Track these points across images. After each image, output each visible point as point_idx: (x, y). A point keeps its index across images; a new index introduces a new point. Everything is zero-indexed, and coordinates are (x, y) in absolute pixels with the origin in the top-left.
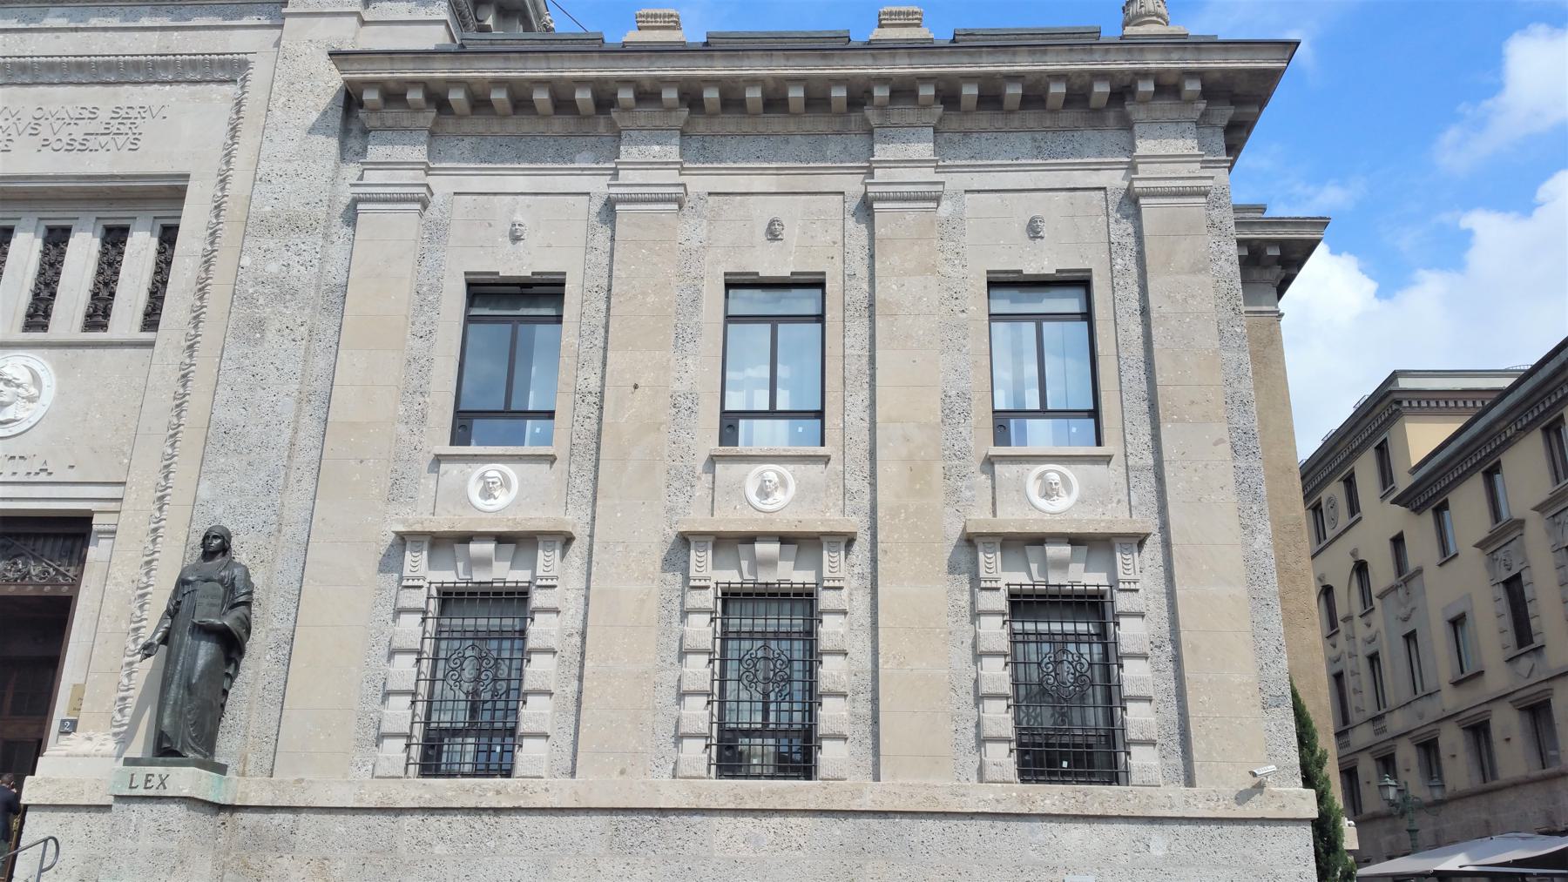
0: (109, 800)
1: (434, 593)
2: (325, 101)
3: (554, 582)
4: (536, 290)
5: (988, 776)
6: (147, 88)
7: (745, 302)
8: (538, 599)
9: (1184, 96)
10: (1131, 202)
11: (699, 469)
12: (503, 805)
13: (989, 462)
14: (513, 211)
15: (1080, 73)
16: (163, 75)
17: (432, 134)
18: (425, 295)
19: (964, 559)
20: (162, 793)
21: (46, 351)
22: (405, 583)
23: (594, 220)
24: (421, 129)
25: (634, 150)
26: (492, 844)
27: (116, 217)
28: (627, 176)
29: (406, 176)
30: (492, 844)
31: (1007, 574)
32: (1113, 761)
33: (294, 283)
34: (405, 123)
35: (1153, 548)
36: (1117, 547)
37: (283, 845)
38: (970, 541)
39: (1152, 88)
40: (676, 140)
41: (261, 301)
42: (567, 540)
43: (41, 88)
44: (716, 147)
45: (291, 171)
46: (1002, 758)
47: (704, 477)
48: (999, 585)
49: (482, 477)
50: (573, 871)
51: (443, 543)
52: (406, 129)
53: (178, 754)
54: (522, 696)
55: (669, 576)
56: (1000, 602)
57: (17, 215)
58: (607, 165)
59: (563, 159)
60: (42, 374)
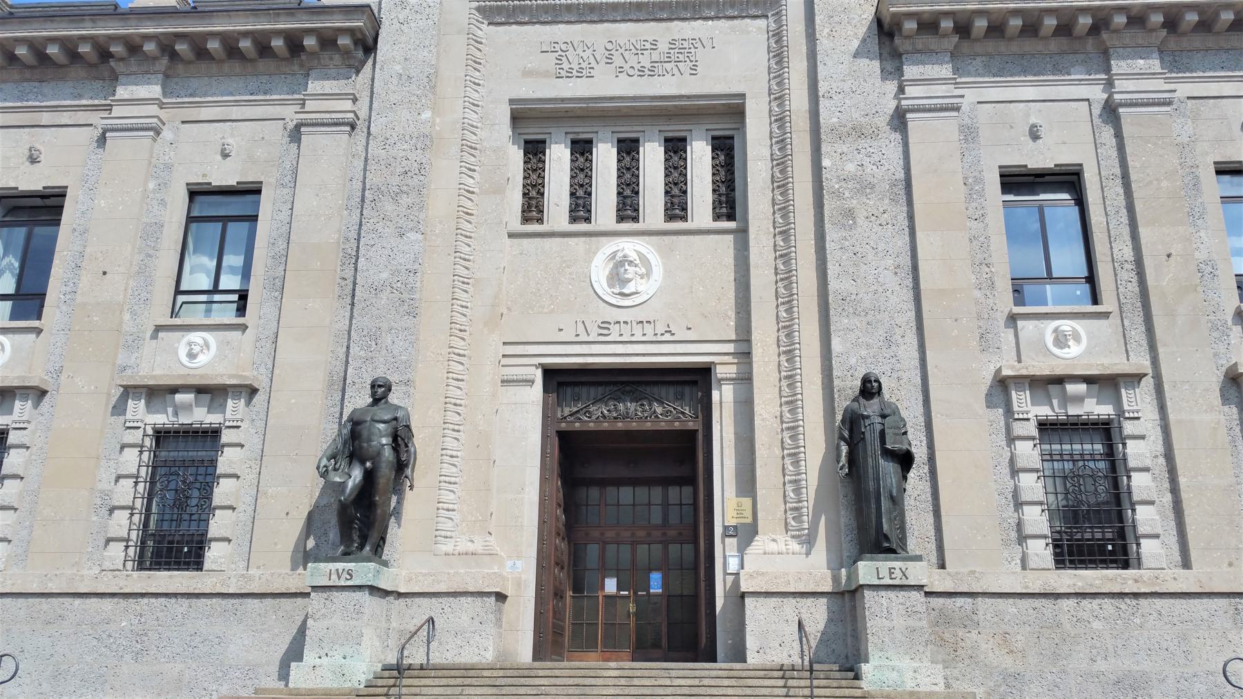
0: (309, 590)
1: (150, 432)
2: (862, 31)
3: (239, 424)
4: (1047, 178)
5: (1032, 564)
6: (693, 23)
7: (206, 207)
8: (226, 437)
9: (1149, 26)
10: (1111, 112)
11: (1230, 323)
12: (1143, 590)
13: (1012, 319)
14: (1028, 115)
15: (1034, 9)
16: (521, 18)
17: (167, 76)
18: (972, 186)
19: (999, 398)
20: (905, 582)
21: (647, 238)
22: (128, 424)
23: (1097, 121)
24: (945, 51)
25: (1123, 63)
26: (1138, 621)
27: (675, 130)
28: (310, 105)
29: (940, 90)
30: (1138, 621)
31: (1031, 409)
32: (1125, 550)
33: (870, 179)
34: (932, 47)
35: (1148, 382)
36: (1122, 384)
37: (969, 622)
38: (1003, 385)
39: (1125, 20)
40: (1156, 55)
41: (847, 195)
42: (253, 391)
43: (606, 24)
44: (1185, 61)
45: (847, 89)
46: (1041, 551)
47: (1234, 328)
48: (1030, 416)
49: (1056, 330)
50: (1209, 642)
51: (156, 394)
52: (932, 51)
53: (894, 552)
54: (211, 510)
55: (1226, 408)
56: (1031, 429)
57: (595, 129)
58: (1098, 76)
59: (1060, 72)
60: (649, 256)
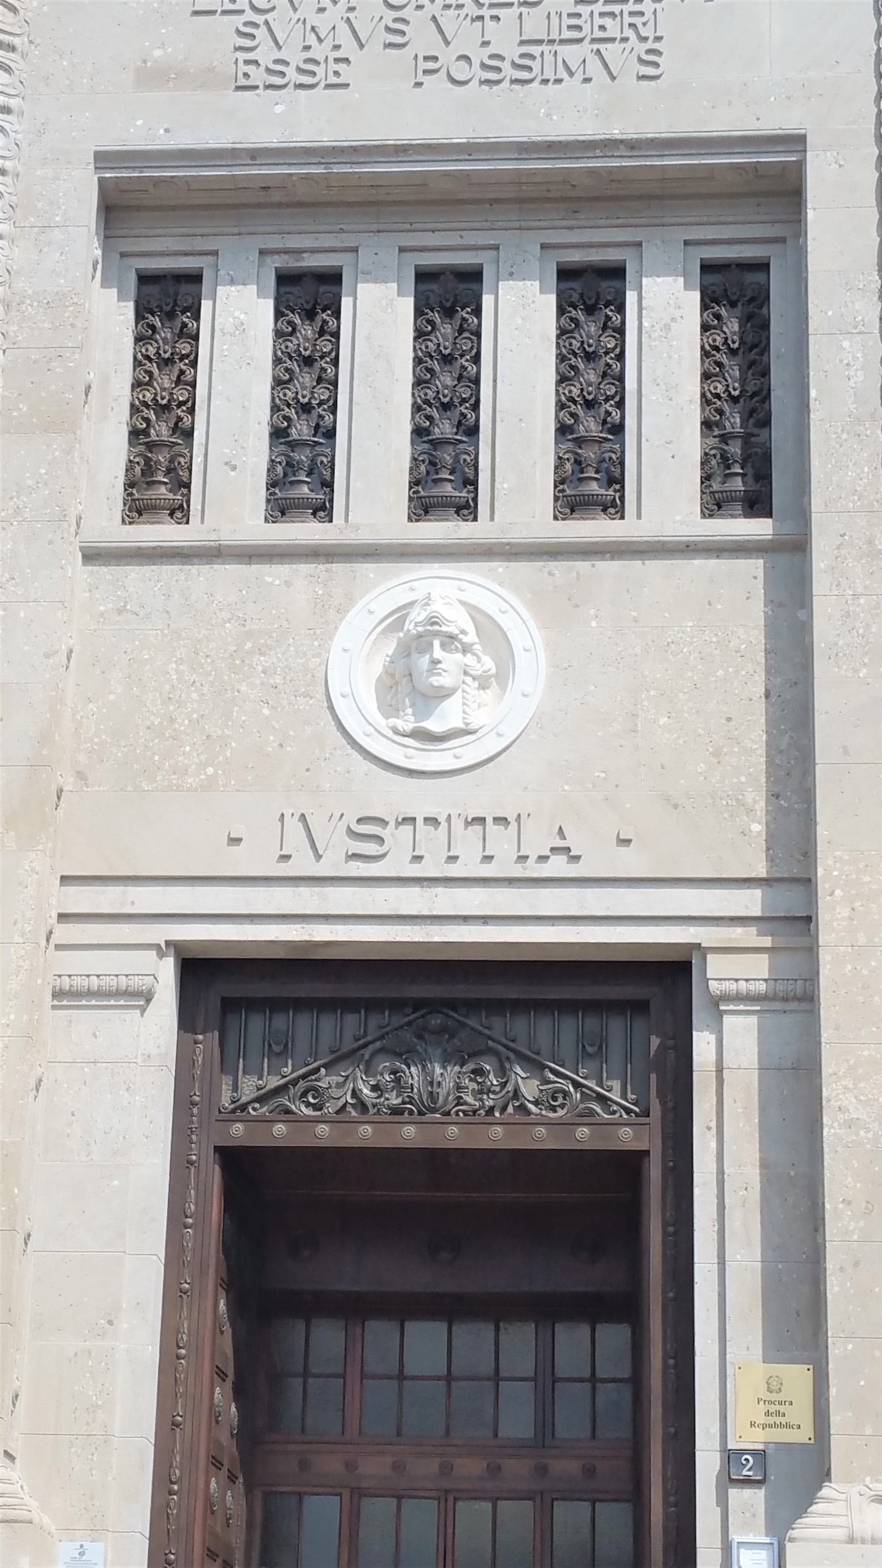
21: (499, 567)
57: (350, 241)
60: (506, 622)
